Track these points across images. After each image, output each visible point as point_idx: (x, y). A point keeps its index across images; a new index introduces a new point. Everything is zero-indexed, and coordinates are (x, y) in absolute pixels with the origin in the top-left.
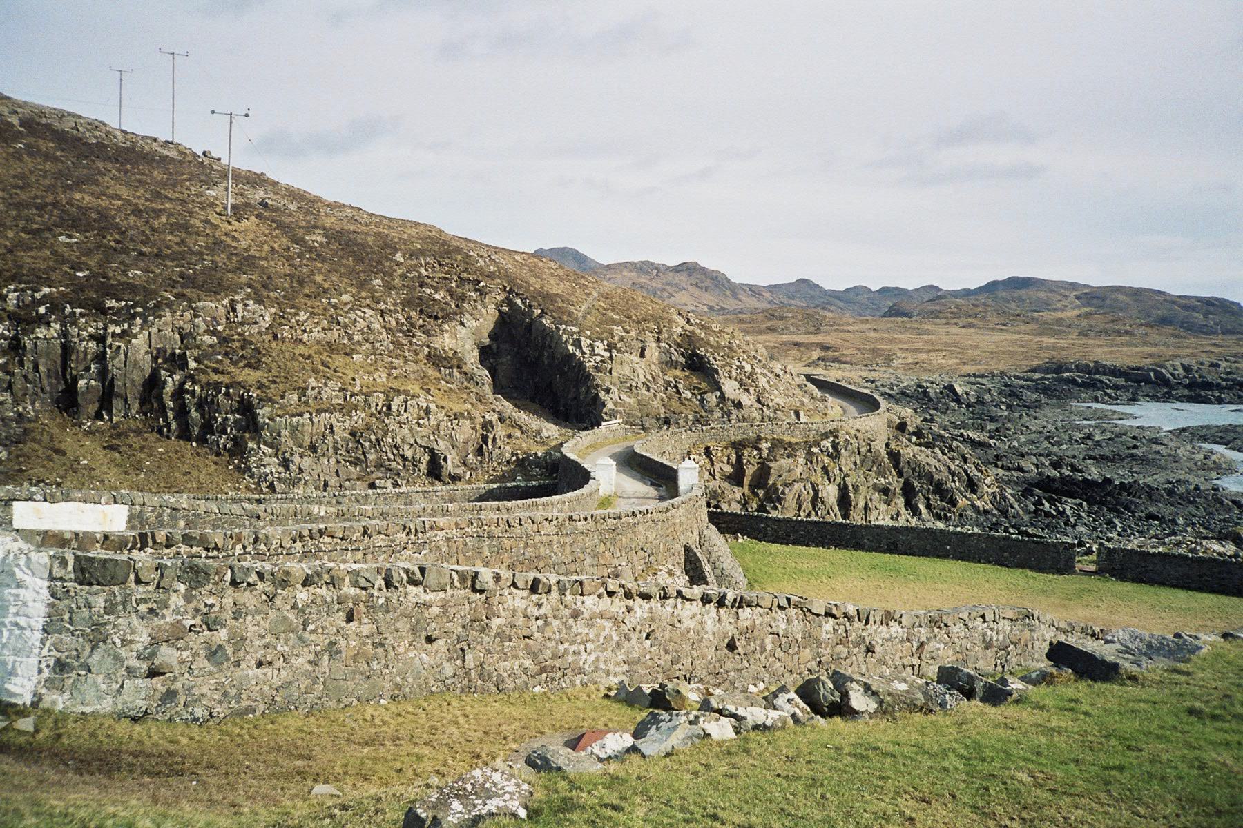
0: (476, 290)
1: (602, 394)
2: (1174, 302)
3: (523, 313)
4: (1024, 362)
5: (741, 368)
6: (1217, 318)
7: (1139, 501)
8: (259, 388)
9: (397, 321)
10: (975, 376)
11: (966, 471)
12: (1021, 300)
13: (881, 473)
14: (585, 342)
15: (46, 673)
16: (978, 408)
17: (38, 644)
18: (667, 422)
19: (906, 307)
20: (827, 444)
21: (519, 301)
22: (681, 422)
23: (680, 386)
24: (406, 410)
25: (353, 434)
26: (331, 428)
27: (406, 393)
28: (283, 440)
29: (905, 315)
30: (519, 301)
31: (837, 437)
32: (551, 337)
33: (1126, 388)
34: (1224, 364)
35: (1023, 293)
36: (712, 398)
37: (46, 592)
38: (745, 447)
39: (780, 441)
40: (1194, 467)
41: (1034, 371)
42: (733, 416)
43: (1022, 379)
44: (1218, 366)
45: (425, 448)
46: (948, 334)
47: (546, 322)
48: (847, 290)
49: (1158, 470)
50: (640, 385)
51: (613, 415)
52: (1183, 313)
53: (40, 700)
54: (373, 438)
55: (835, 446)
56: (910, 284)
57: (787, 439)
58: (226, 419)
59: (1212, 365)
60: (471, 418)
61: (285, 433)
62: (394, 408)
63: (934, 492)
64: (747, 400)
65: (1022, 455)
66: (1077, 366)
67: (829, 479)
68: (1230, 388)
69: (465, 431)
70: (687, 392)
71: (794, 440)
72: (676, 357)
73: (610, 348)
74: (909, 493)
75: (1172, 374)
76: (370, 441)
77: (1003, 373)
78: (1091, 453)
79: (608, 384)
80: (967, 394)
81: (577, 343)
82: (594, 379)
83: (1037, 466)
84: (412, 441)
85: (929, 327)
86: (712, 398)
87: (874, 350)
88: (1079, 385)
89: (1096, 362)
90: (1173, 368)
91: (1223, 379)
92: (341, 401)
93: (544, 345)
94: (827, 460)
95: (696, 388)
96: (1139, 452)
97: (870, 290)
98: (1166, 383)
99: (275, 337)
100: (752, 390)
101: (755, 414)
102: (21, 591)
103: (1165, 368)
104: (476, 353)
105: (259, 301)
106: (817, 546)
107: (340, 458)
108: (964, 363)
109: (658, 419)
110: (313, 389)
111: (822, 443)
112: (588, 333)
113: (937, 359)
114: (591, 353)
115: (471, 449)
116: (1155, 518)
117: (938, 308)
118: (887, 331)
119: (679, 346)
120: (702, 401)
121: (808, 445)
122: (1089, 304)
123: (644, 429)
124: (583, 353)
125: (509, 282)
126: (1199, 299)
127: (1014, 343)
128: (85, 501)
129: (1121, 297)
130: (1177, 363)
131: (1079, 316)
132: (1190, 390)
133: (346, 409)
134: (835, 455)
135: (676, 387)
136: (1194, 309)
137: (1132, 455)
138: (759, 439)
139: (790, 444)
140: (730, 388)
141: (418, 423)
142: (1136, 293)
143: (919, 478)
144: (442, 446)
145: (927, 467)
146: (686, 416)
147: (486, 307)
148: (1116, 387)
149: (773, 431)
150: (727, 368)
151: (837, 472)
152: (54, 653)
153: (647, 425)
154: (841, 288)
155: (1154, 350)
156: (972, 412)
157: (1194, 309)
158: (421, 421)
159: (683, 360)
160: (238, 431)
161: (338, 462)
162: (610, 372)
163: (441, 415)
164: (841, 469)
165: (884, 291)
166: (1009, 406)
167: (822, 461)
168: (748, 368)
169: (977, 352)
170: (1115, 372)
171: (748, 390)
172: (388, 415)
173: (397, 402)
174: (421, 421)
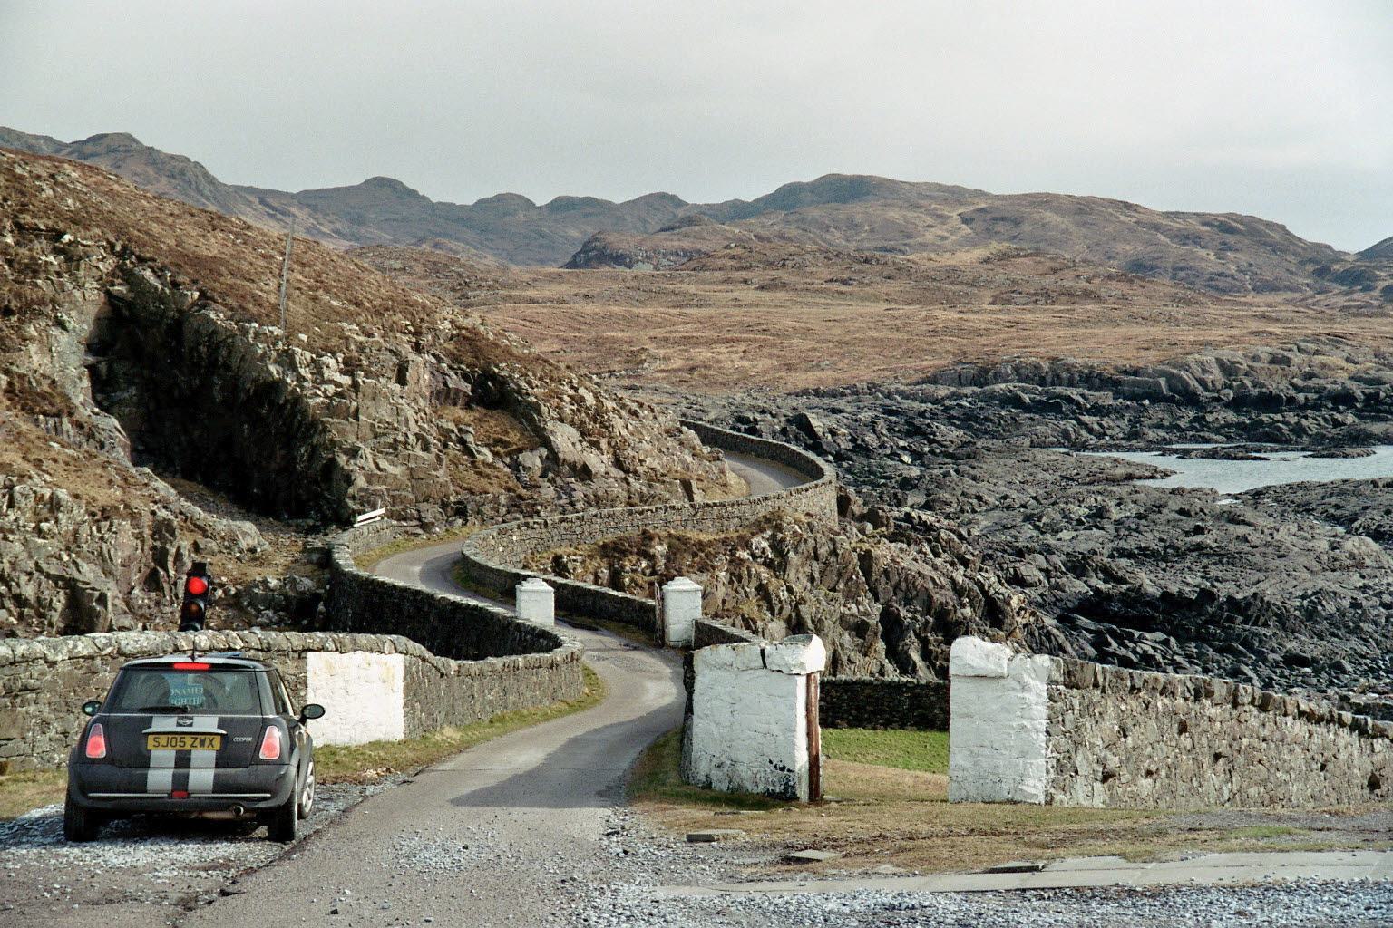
0: (56, 251)
1: (342, 460)
2: (1156, 227)
3: (161, 298)
4: (909, 363)
5: (579, 401)
6: (1243, 258)
7: (1268, 632)
10: (817, 393)
11: (980, 585)
12: (853, 226)
13: (851, 596)
14: (303, 356)
15: (1052, 775)
16: (859, 461)
17: (1044, 745)
18: (461, 511)
19: (619, 241)
22: (486, 509)
23: (470, 439)
29: (619, 259)
30: (148, 273)
31: (779, 528)
32: (230, 349)
33: (1118, 412)
34: (1297, 358)
35: (857, 210)
36: (533, 460)
37: (1045, 695)
38: (624, 553)
39: (683, 540)
40: (1317, 567)
41: (933, 380)
42: (578, 495)
43: (912, 397)
44: (1287, 361)
46: (737, 303)
47: (217, 316)
48: (482, 204)
49: (1261, 575)
50: (412, 438)
51: (368, 501)
52: (1176, 251)
53: (1052, 799)
55: (777, 545)
56: (618, 193)
57: (693, 535)
60: (134, 517)
63: (935, 629)
64: (598, 462)
65: (1020, 553)
67: (771, 610)
68: (1316, 407)
69: (125, 542)
70: (484, 450)
71: (705, 537)
72: (455, 381)
73: (349, 367)
74: (892, 628)
75: (1202, 382)
77: (873, 387)
78: (1123, 544)
79: (351, 439)
80: (833, 433)
81: (287, 360)
82: (325, 430)
83: (1047, 573)
84: (31, 565)
85: (692, 289)
86: (533, 460)
87: (597, 342)
88: (1026, 408)
89: (1055, 359)
90: (1202, 367)
91: (1298, 389)
93: (213, 363)
94: (765, 573)
95: (498, 442)
96: (1208, 539)
97: (533, 204)
98: (1190, 399)
100: (603, 442)
101: (617, 490)
102: (1026, 695)
104: (86, 383)
106: (851, 726)
108: (789, 368)
109: (444, 506)
111: (755, 541)
112: (304, 337)
113: (731, 359)
114: (318, 382)
115: (136, 577)
116: (1303, 662)
117: (686, 244)
118: (613, 298)
119: (456, 359)
120: (515, 466)
121: (730, 547)
122: (990, 233)
123: (425, 526)
124: (301, 379)
125: (120, 232)
126: (1206, 219)
127: (878, 321)
128: (371, 650)
129: (1050, 217)
130: (1209, 357)
131: (987, 260)
132: (1238, 412)
134: (778, 565)
135: (462, 441)
136: (1196, 239)
137: (1198, 547)
138: (647, 537)
140: (565, 439)
141: (39, 532)
142: (1083, 208)
143: (907, 602)
144: (88, 573)
145: (919, 581)
146: (496, 498)
147: (81, 287)
148: (1098, 410)
149: (667, 523)
150: (555, 401)
151: (784, 595)
152: (1055, 754)
153: (429, 518)
154: (466, 196)
155: (1157, 331)
156: (849, 471)
157: (1196, 239)
158: (45, 526)
159: (467, 387)
162: (356, 415)
163: (80, 512)
164: (790, 590)
165: (562, 206)
166: (917, 456)
167: (758, 575)
168: (590, 400)
169: (811, 344)
170: (1092, 379)
171: (596, 445)
174: (45, 526)
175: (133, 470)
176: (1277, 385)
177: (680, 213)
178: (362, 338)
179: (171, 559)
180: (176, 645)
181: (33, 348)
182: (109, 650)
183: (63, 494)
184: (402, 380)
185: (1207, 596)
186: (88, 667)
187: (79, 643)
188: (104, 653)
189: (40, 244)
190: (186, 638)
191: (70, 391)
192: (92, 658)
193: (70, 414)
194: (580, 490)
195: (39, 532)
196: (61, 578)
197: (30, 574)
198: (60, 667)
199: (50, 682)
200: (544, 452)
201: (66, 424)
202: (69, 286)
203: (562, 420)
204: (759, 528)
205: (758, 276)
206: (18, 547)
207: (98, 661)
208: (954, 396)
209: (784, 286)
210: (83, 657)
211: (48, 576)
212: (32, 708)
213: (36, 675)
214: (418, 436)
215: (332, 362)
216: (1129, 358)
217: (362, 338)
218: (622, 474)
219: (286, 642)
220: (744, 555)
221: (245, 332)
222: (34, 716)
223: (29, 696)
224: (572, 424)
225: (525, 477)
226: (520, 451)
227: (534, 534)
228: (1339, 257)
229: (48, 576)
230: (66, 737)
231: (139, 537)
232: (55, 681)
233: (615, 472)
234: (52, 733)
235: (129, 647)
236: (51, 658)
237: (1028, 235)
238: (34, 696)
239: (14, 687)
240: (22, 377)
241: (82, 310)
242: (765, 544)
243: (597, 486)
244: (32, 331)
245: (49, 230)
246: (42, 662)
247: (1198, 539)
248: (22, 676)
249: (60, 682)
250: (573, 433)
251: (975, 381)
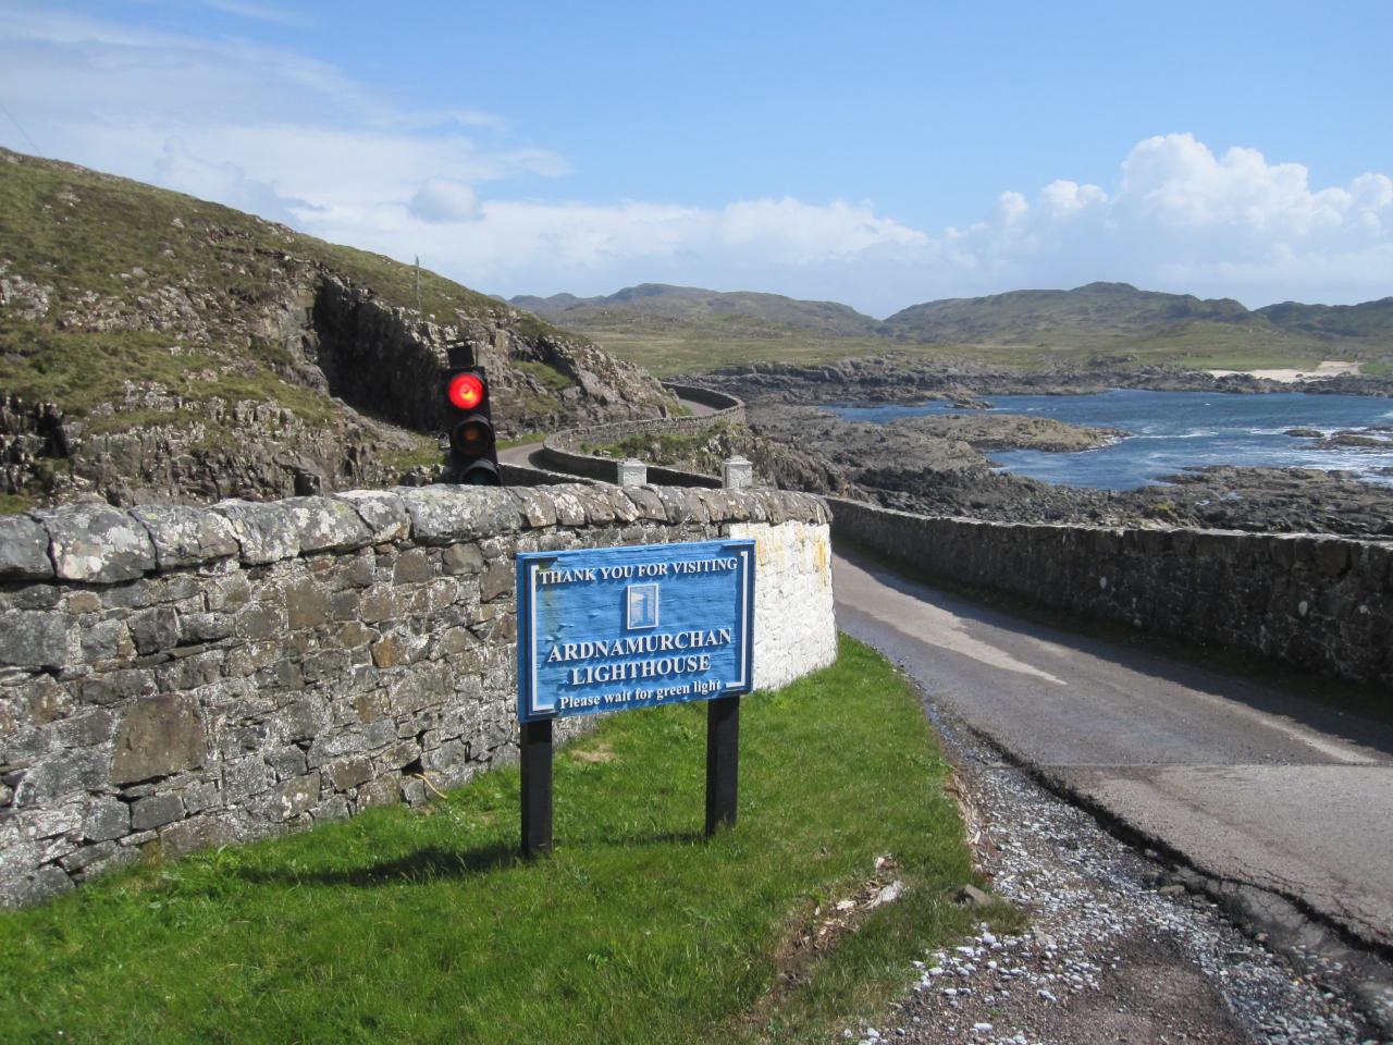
2: (796, 307)
5: (596, 357)
8: (58, 395)
9: (208, 303)
14: (433, 328)
20: (714, 441)
21: (336, 279)
23: (533, 381)
24: (255, 419)
25: (195, 454)
26: (167, 447)
27: (253, 395)
28: (105, 466)
31: (724, 432)
36: (572, 393)
41: (716, 373)
42: (600, 415)
45: (286, 468)
50: (502, 379)
54: (221, 457)
55: (724, 443)
58: (17, 441)
59: (877, 362)
61: (107, 456)
62: (241, 417)
64: (611, 394)
66: (756, 367)
69: (327, 441)
76: (219, 462)
81: (424, 331)
86: (572, 393)
90: (844, 365)
92: (171, 409)
95: (551, 382)
98: (839, 381)
99: (61, 326)
100: (613, 382)
101: (623, 411)
103: (836, 365)
105: (29, 277)
107: (184, 487)
109: (521, 421)
110: (133, 393)
112: (433, 316)
115: (337, 467)
133: (178, 421)
135: (529, 383)
138: (649, 438)
139: (679, 443)
140: (589, 380)
141: (274, 437)
144: (307, 464)
147: (295, 287)
153: (513, 429)
159: (529, 350)
160: (36, 457)
161: (182, 493)
170: (794, 372)
171: (609, 384)
172: (234, 426)
173: (242, 408)
175: (331, 400)
176: (878, 374)
177: (575, 302)
178: (467, 318)
179: (358, 455)
180: (525, 518)
181: (267, 322)
182: (392, 530)
183: (288, 412)
184: (492, 342)
185: (973, 471)
186: (345, 574)
187: (323, 514)
188: (380, 537)
189: (271, 261)
190: (542, 501)
191: (290, 349)
192: (354, 549)
193: (291, 364)
194: (601, 412)
195: (274, 437)
196: (290, 467)
197: (269, 465)
198: (281, 577)
199: (256, 615)
200: (578, 388)
201: (289, 370)
202: (288, 286)
203: (587, 369)
204: (712, 432)
205: (619, 327)
206: (261, 446)
207: (369, 557)
208: (728, 380)
209: (632, 332)
210: (334, 550)
211: (282, 466)
212: (215, 690)
213: (219, 598)
214: (506, 378)
215: (451, 331)
216: (809, 361)
217: (467, 318)
218: (624, 402)
219: (699, 505)
220: (705, 449)
221: (396, 313)
222: (221, 709)
223: (205, 656)
224: (593, 372)
225: (567, 403)
226: (564, 388)
227: (581, 437)
228: (876, 322)
229: (282, 466)
230: (305, 748)
231: (338, 440)
232: (268, 614)
233: (621, 401)
234: (270, 745)
235: (435, 523)
236: (254, 553)
237: (732, 310)
238: (219, 655)
239: (161, 637)
240: (261, 339)
241: (300, 299)
242: (716, 443)
243: (611, 409)
244: (266, 310)
245: (277, 253)
246: (232, 565)
247: (885, 444)
248: (182, 605)
249: (283, 615)
250: (594, 377)
251: (737, 374)
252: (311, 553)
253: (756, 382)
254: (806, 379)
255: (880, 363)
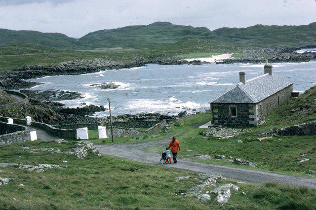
59: (72, 63)
252: (113, 141)
253: (30, 73)
254: (48, 71)
255: (74, 63)
